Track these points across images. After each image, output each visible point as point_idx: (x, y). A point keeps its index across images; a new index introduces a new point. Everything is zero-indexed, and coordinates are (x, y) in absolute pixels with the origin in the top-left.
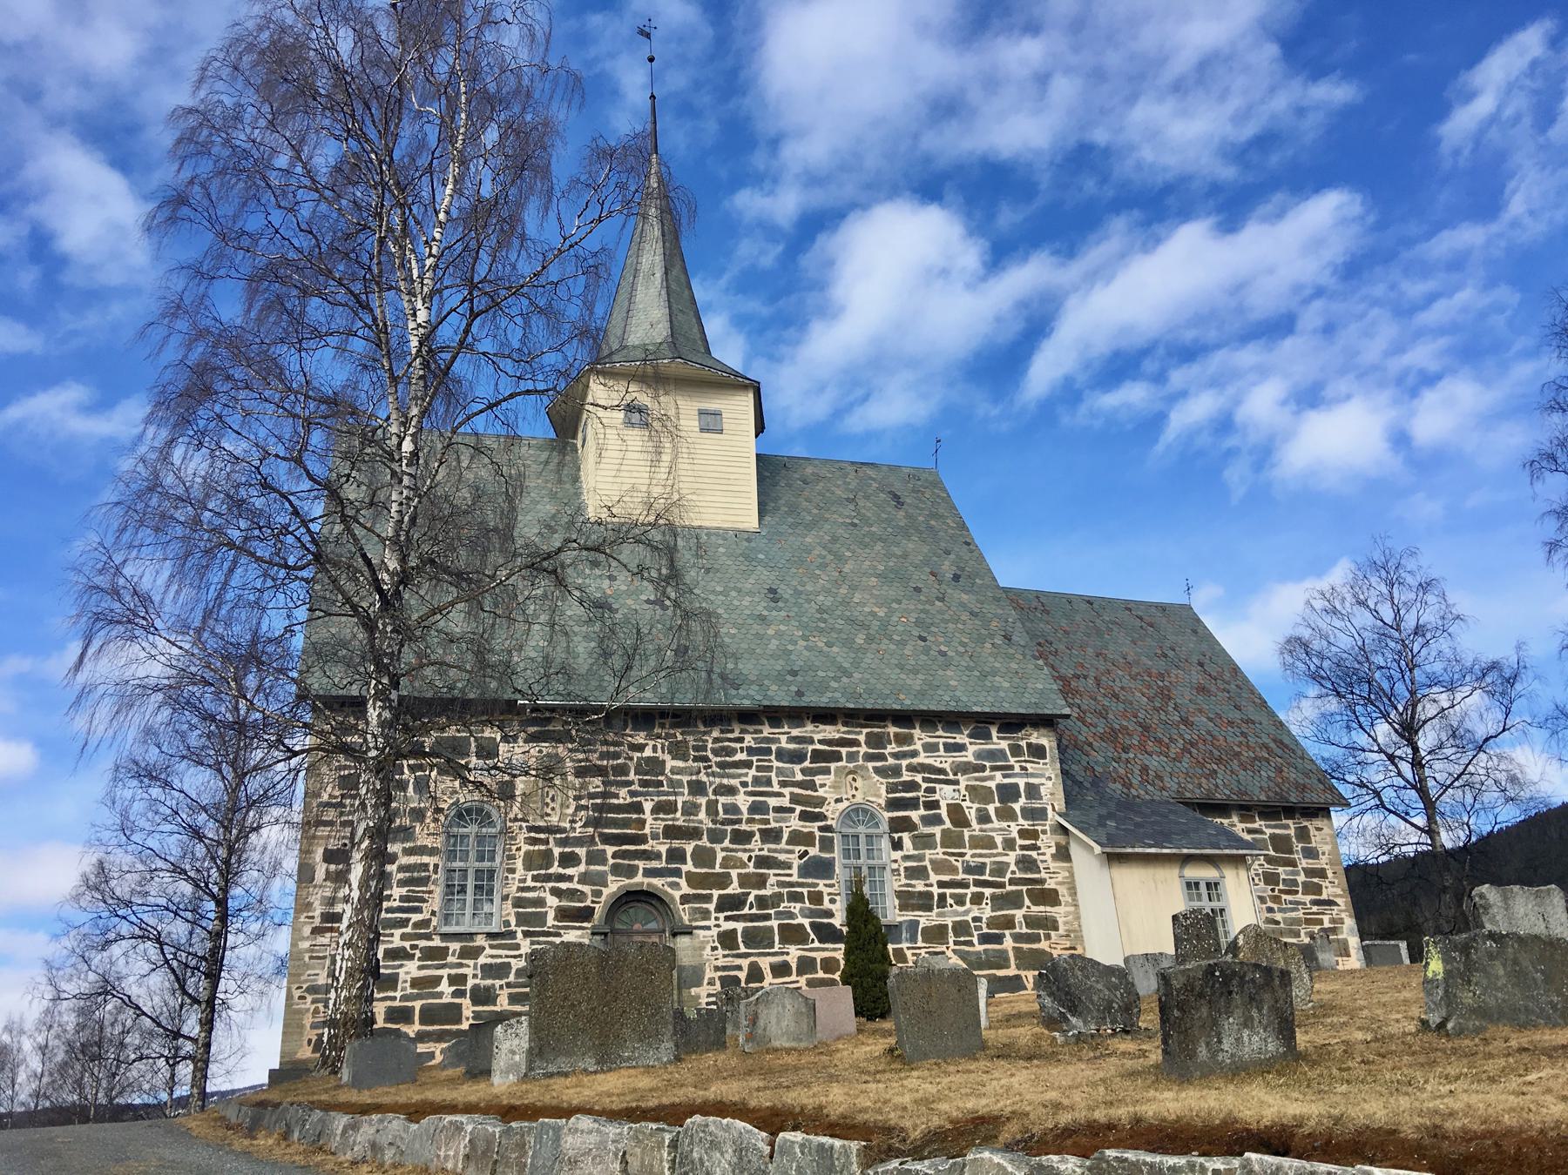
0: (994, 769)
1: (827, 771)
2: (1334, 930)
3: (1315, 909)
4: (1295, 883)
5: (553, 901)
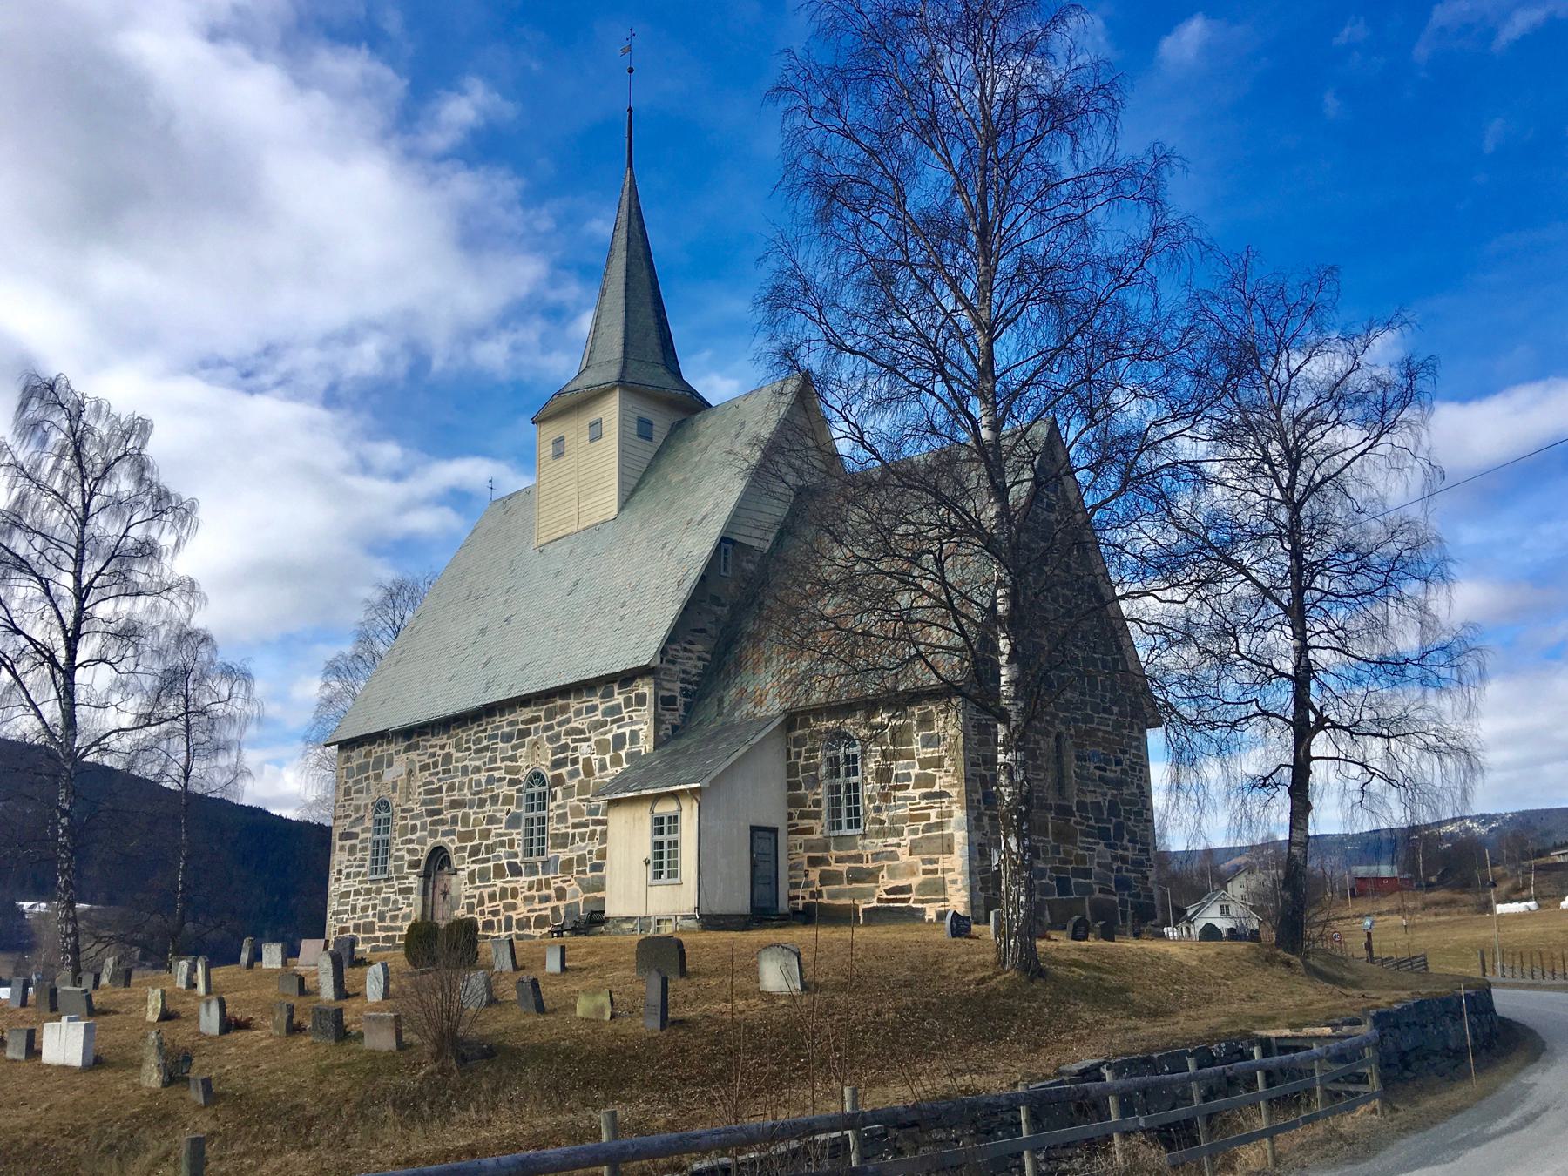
0: (613, 722)
1: (523, 745)
2: (940, 825)
3: (923, 803)
4: (907, 777)
5: (407, 857)
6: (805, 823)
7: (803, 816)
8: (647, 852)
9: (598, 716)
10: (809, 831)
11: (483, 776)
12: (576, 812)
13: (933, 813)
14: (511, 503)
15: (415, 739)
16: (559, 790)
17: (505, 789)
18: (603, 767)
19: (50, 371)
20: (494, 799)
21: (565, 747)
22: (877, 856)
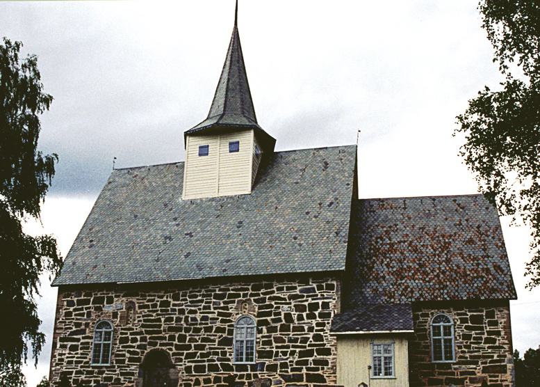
1: (234, 302)
5: (128, 355)
13: (495, 356)
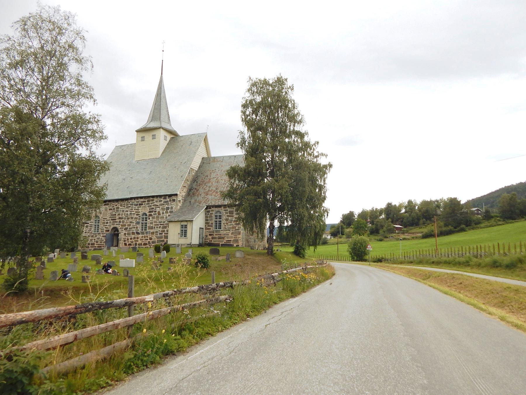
2: (238, 230)
6: (209, 227)
7: (208, 226)
8: (179, 232)
9: (162, 202)
10: (210, 229)
11: (129, 213)
12: (155, 222)
14: (123, 148)
15: (107, 203)
16: (151, 217)
17: (135, 216)
18: (163, 213)
19: (382, 242)
20: (132, 218)
21: (153, 208)
22: (224, 234)
